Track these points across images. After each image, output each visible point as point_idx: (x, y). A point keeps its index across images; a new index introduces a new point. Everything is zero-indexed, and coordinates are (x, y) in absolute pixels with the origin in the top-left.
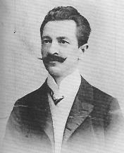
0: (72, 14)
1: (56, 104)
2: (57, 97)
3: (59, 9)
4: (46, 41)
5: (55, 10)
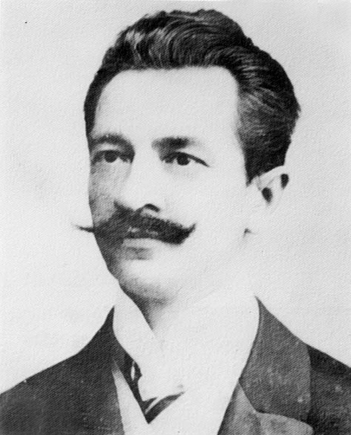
0: (222, 44)
1: (150, 417)
2: (150, 389)
3: (161, 20)
4: (110, 156)
5: (146, 25)
